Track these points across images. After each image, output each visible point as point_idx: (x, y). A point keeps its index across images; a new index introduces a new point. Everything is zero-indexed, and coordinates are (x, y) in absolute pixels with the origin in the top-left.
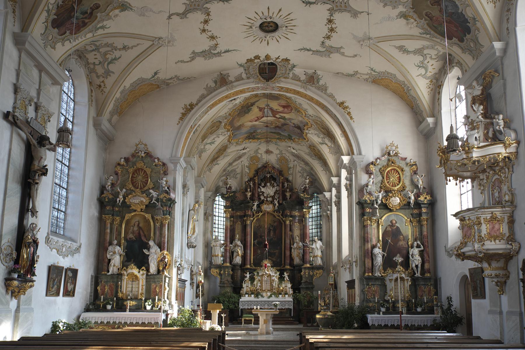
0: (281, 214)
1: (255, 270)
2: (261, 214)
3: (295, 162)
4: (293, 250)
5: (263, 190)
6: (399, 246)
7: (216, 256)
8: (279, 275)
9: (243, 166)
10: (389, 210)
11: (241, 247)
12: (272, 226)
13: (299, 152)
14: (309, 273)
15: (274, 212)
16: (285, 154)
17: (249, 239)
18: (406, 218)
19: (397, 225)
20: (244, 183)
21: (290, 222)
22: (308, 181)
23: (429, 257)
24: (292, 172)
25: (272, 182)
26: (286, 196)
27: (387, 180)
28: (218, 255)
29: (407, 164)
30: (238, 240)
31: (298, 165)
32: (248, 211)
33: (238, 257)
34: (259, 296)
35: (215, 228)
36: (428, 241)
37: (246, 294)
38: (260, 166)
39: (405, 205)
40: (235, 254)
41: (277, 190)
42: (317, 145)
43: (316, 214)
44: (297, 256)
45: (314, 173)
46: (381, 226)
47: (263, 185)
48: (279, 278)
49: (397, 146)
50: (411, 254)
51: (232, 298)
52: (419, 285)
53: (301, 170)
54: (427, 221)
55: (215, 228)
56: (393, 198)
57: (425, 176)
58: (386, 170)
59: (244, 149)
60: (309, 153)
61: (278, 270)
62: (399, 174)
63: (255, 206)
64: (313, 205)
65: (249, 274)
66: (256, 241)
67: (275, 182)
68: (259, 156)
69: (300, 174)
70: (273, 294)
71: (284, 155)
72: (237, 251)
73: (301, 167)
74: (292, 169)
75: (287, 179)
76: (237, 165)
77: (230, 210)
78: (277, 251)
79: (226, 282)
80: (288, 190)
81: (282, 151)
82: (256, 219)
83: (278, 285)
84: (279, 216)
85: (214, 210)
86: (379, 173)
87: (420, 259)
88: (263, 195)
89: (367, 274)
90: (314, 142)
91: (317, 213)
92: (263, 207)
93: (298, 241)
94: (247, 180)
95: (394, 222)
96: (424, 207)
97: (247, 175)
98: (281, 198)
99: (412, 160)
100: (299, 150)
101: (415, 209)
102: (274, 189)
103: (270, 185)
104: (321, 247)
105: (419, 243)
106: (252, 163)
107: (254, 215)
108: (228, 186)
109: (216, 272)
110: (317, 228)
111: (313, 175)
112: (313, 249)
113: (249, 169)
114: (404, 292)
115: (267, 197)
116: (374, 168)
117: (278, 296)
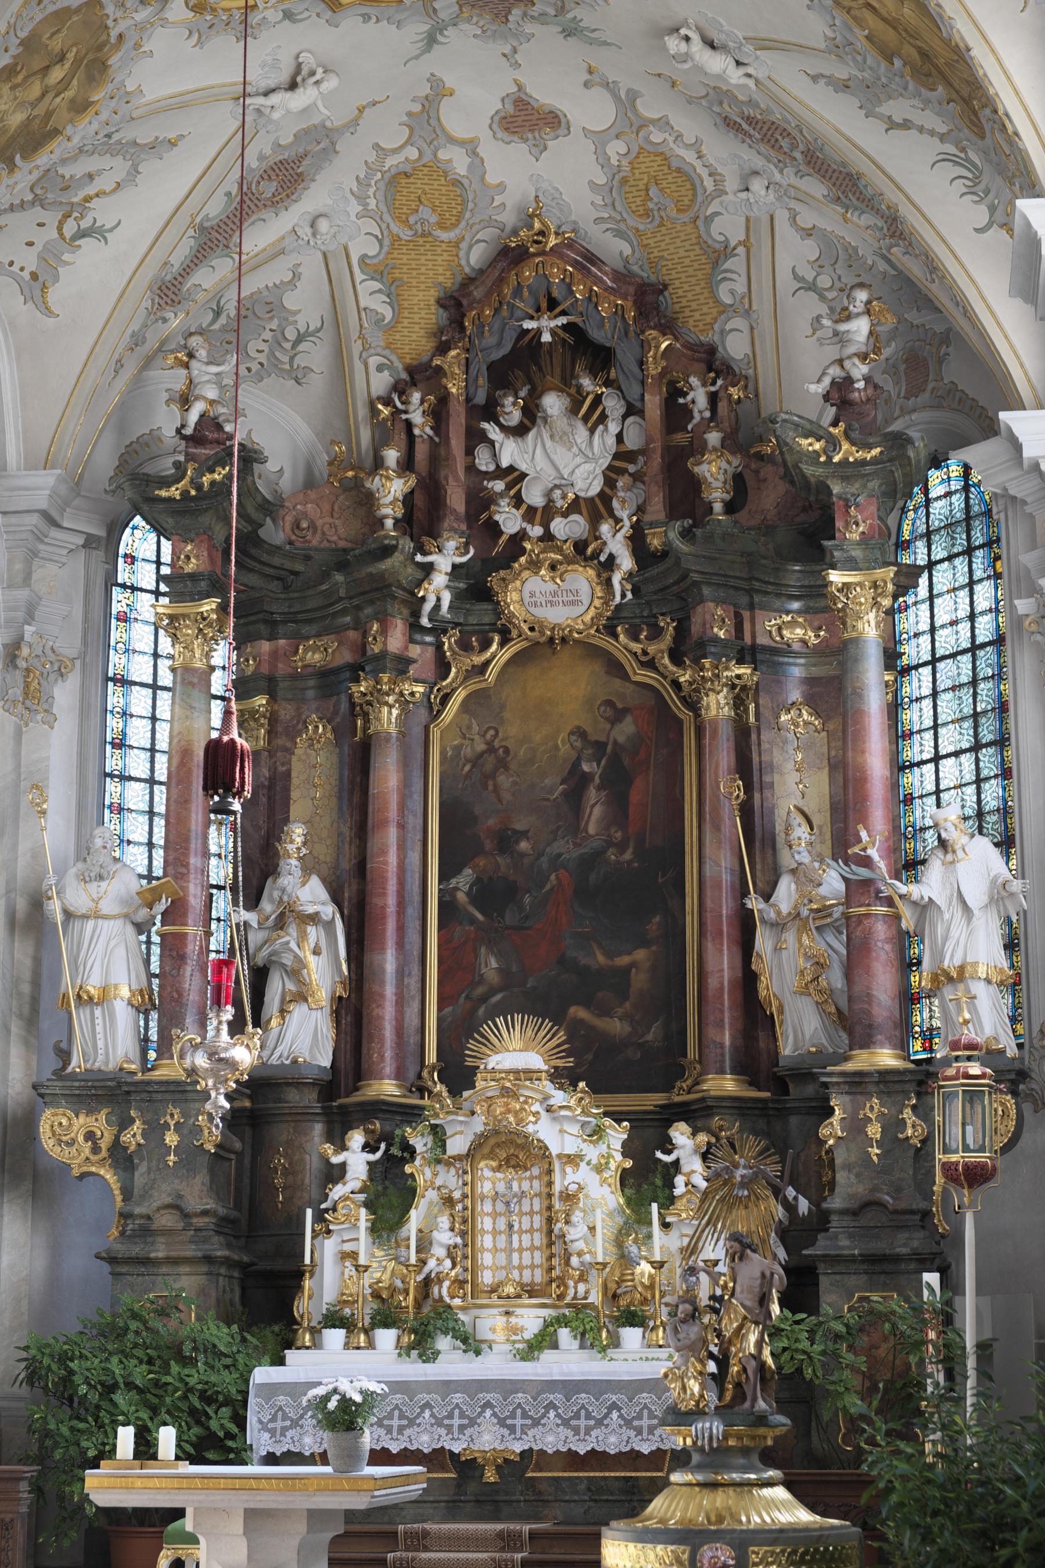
1: (411, 1114)
2: (499, 655)
3: (757, 185)
4: (763, 942)
5: (510, 451)
7: (84, 1000)
8: (627, 1150)
9: (338, 266)
11: (329, 925)
12: (600, 747)
14: (893, 1126)
15: (611, 631)
16: (663, 123)
17: (392, 858)
20: (362, 412)
21: (738, 704)
22: (860, 328)
24: (741, 288)
25: (586, 383)
26: (695, 484)
28: (104, 998)
30: (307, 870)
31: (782, 217)
32: (384, 631)
33: (298, 1011)
34: (443, 1343)
35: (125, 778)
37: (334, 1320)
38: (476, 256)
40: (276, 987)
41: (633, 441)
43: (964, 628)
44: (804, 991)
45: (915, 269)
47: (513, 416)
48: (625, 1177)
51: (187, 1361)
53: (818, 265)
55: (125, 778)
59: (293, 86)
60: (837, 49)
61: (618, 1118)
63: (440, 580)
64: (939, 553)
65: (369, 1147)
66: (464, 880)
67: (608, 383)
68: (459, 163)
69: (811, 306)
70: (561, 1321)
71: (657, 137)
72: (287, 960)
74: (736, 264)
75: (711, 351)
76: (278, 252)
78: (640, 954)
79: (167, 1220)
80: (713, 438)
81: (633, 96)
82: (460, 696)
83: (619, 1243)
84: (650, 664)
85: (114, 636)
88: (518, 501)
91: (972, 617)
92: (512, 596)
93: (805, 858)
94: (381, 382)
97: (377, 339)
98: (657, 509)
100: (764, 44)
102: (604, 443)
103: (574, 409)
104: (999, 894)
106: (406, 234)
107: (443, 667)
108: (193, 417)
109: (90, 1136)
110: (976, 747)
111: (925, 302)
112: (925, 908)
113: (394, 291)
115: (548, 512)
117: (615, 1342)
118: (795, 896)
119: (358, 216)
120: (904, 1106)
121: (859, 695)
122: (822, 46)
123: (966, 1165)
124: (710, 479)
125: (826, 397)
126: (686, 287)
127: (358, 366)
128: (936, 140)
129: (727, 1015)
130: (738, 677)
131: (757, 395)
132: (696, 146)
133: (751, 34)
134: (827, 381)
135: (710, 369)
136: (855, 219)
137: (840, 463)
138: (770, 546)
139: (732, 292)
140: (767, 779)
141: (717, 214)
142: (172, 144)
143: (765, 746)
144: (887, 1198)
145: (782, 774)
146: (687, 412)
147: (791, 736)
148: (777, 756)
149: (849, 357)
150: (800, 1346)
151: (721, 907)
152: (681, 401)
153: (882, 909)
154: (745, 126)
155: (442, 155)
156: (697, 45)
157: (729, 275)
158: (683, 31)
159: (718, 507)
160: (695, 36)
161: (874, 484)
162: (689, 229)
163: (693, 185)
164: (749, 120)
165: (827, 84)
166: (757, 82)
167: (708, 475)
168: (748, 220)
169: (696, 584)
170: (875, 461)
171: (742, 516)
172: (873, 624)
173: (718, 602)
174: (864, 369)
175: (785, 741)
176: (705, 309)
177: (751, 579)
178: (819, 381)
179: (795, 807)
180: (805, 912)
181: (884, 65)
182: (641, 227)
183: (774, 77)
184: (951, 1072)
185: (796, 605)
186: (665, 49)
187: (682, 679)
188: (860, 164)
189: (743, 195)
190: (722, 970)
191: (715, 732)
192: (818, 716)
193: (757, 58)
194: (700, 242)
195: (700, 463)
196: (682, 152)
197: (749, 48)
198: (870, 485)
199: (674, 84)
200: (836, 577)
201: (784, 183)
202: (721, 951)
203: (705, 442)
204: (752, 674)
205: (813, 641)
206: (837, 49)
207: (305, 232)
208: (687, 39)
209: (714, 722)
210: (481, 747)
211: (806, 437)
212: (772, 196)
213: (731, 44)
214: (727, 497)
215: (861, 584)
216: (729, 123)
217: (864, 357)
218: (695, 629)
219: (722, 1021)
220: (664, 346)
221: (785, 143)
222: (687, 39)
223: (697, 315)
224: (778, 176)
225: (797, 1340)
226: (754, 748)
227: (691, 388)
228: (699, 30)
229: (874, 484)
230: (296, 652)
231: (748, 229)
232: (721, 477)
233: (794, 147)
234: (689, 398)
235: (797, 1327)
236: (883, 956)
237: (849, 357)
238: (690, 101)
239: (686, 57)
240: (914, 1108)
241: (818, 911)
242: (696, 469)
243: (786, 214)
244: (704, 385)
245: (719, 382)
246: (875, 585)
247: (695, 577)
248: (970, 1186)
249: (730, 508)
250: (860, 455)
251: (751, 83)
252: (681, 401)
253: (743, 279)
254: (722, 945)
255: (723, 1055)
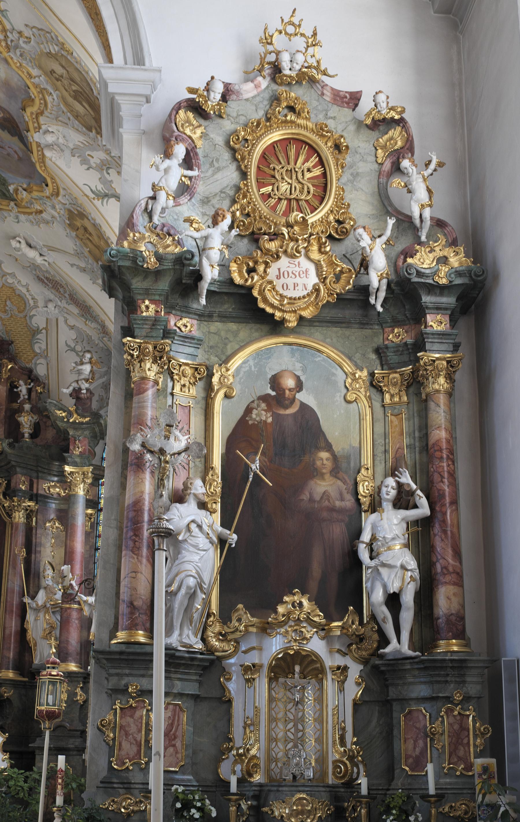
3: (51, 306)
4: (30, 617)
6: (311, 500)
10: (265, 328)
13: (52, 257)
14: (72, 695)
16: (13, 275)
18: (348, 367)
19: (302, 397)
22: (87, 368)
23: (457, 554)
24: (44, 347)
26: (18, 425)
27: (261, 185)
29: (360, 124)
36: (452, 475)
39: (342, 300)
42: (83, 200)
46: (221, 395)
49: (315, 34)
50: (366, 537)
52: (404, 701)
53: (76, 341)
54: (450, 378)
56: (284, 262)
57: (440, 165)
58: (259, 139)
62: (321, 162)
71: (10, 280)
73: (72, 328)
74: (42, 336)
80: (27, 407)
86: (226, 155)
87: (412, 564)
89: (122, 636)
90: (77, 193)
93: (50, 583)
95: (290, 383)
96: (438, 309)
99: (382, 98)
100: (51, 249)
101: (396, 323)
105: (406, 479)
114: (319, 740)
116: (199, 131)
118: (45, 598)
120: (77, 687)
121: (74, 517)
122: (73, 252)
123: (47, 711)
124: (24, 424)
125: (71, 395)
126: (21, 344)
128: (455, 384)
129: (12, 646)
130: (29, 506)
131: (49, 391)
132: (27, 286)
133: (45, 244)
134: (71, 389)
135: (29, 378)
136: (90, 324)
137: (73, 422)
138: (47, 454)
139: (40, 348)
140: (38, 549)
141: (34, 315)
143: (38, 535)
144: (68, 725)
145: (45, 548)
146: (18, 395)
147: (50, 532)
148: (43, 540)
149: (81, 380)
150: (19, 784)
151: (13, 601)
152: (15, 390)
153: (76, 606)
154: (46, 281)
156: (23, 245)
157: (39, 341)
158: (17, 239)
159: (26, 435)
160: (23, 242)
161: (87, 433)
162: (23, 320)
163: (25, 302)
164: (47, 278)
165: (77, 268)
166: (49, 264)
167: (23, 422)
168: (47, 319)
169: (13, 466)
170: (87, 423)
171: (38, 440)
172: (82, 489)
173: (23, 474)
174: (87, 385)
175: (48, 534)
176: (29, 354)
177: (37, 466)
178: (68, 388)
179: (48, 562)
180: (48, 605)
181: (95, 264)
182: (3, 317)
183: (56, 262)
184: (44, 673)
185: (56, 479)
186: (11, 245)
187: (5, 505)
188: (91, 303)
189: (45, 309)
190: (12, 627)
191: (17, 528)
192: (62, 525)
193: (49, 254)
194: (27, 325)
195: (20, 417)
196: (20, 288)
197: (45, 249)
198: (85, 433)
199: (16, 260)
200: (67, 468)
201: (62, 306)
202: (12, 619)
203: (23, 408)
204: (35, 506)
205: (63, 494)
206: (78, 254)
208: (20, 242)
209: (17, 524)
211: (59, 410)
212: (57, 311)
213: (38, 247)
214: (31, 432)
215: (78, 473)
216: (39, 279)
217: (87, 380)
218: (13, 485)
219: (10, 647)
220: (9, 367)
221: (61, 290)
222: (20, 242)
223: (25, 356)
224: (59, 303)
225: (19, 781)
226: (34, 536)
227: (20, 386)
228: (25, 239)
229: (87, 433)
231: (47, 323)
232: (29, 423)
233: (65, 292)
234: (19, 389)
235: (19, 776)
236: (74, 625)
237: (81, 380)
238: (24, 267)
239: (19, 250)
240: (81, 688)
241: (53, 605)
242: (19, 419)
243: (63, 319)
244: (26, 384)
245: (32, 384)
246: (84, 474)
247: (13, 463)
248: (49, 720)
249: (33, 436)
250: (81, 420)
251: (46, 264)
252: (15, 390)
253: (45, 343)
254: (12, 616)
255: (9, 662)
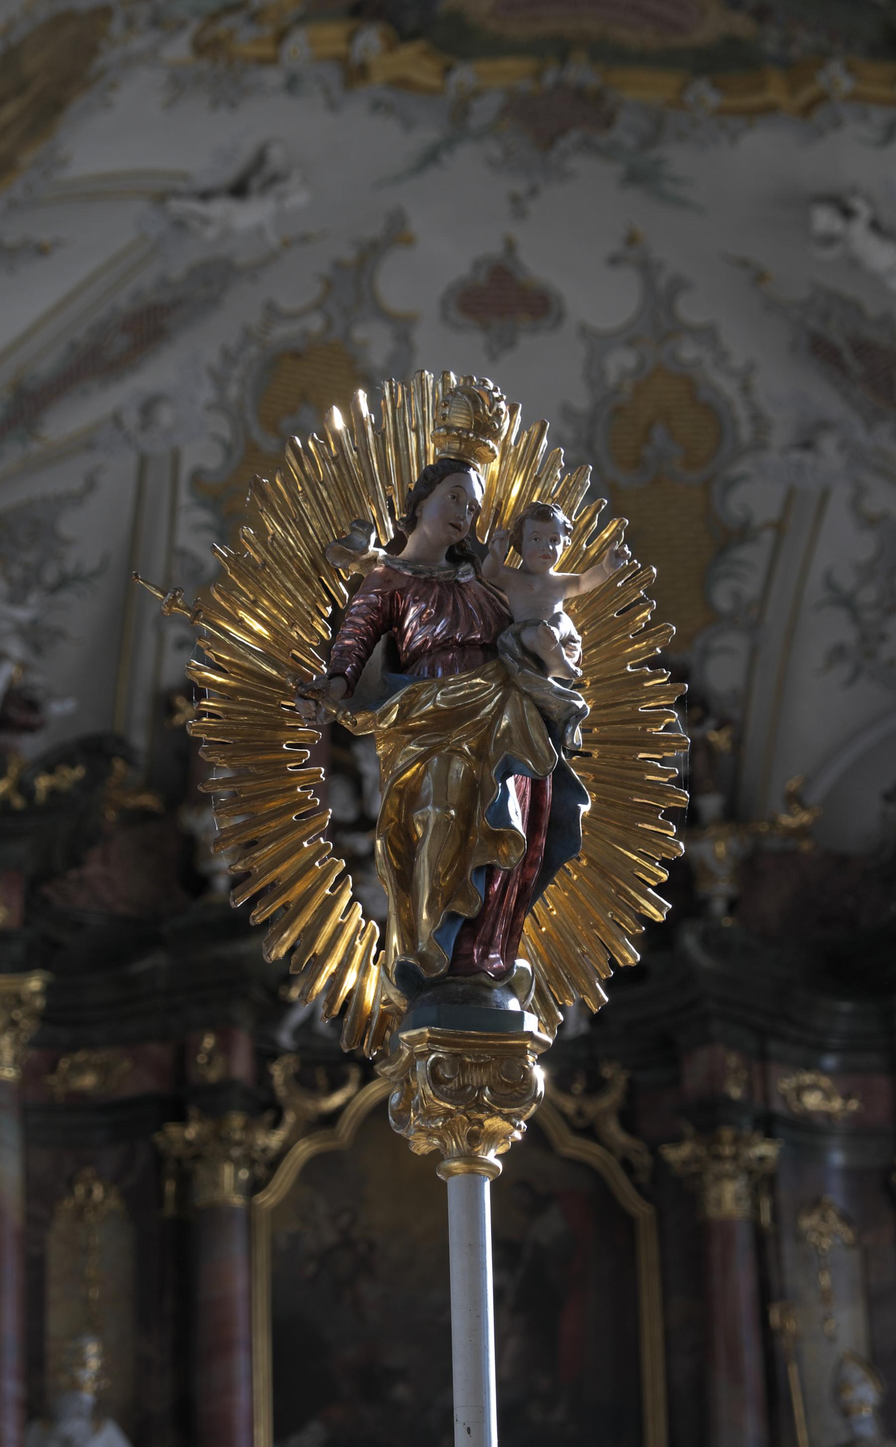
0: (610, 1100)
3: (828, 444)
20: (141, 708)
24: (751, 588)
31: (842, 493)
32: (225, 1046)
71: (688, 352)
77: (35, 984)
81: (678, 285)
119: (210, 407)
127: (149, 638)
139: (736, 596)
141: (743, 478)
142: (42, 251)
155: (359, 333)
164: (862, 348)
189: (796, 456)
207: (132, 419)
210: (330, 1237)
230: (53, 1068)
249: (733, 906)
